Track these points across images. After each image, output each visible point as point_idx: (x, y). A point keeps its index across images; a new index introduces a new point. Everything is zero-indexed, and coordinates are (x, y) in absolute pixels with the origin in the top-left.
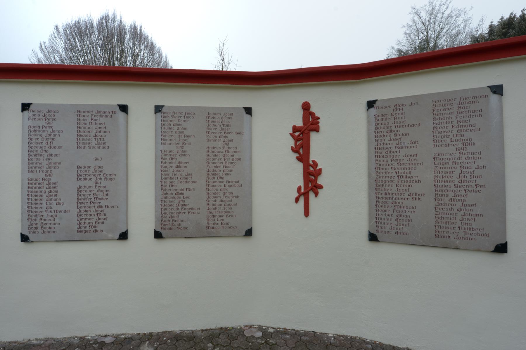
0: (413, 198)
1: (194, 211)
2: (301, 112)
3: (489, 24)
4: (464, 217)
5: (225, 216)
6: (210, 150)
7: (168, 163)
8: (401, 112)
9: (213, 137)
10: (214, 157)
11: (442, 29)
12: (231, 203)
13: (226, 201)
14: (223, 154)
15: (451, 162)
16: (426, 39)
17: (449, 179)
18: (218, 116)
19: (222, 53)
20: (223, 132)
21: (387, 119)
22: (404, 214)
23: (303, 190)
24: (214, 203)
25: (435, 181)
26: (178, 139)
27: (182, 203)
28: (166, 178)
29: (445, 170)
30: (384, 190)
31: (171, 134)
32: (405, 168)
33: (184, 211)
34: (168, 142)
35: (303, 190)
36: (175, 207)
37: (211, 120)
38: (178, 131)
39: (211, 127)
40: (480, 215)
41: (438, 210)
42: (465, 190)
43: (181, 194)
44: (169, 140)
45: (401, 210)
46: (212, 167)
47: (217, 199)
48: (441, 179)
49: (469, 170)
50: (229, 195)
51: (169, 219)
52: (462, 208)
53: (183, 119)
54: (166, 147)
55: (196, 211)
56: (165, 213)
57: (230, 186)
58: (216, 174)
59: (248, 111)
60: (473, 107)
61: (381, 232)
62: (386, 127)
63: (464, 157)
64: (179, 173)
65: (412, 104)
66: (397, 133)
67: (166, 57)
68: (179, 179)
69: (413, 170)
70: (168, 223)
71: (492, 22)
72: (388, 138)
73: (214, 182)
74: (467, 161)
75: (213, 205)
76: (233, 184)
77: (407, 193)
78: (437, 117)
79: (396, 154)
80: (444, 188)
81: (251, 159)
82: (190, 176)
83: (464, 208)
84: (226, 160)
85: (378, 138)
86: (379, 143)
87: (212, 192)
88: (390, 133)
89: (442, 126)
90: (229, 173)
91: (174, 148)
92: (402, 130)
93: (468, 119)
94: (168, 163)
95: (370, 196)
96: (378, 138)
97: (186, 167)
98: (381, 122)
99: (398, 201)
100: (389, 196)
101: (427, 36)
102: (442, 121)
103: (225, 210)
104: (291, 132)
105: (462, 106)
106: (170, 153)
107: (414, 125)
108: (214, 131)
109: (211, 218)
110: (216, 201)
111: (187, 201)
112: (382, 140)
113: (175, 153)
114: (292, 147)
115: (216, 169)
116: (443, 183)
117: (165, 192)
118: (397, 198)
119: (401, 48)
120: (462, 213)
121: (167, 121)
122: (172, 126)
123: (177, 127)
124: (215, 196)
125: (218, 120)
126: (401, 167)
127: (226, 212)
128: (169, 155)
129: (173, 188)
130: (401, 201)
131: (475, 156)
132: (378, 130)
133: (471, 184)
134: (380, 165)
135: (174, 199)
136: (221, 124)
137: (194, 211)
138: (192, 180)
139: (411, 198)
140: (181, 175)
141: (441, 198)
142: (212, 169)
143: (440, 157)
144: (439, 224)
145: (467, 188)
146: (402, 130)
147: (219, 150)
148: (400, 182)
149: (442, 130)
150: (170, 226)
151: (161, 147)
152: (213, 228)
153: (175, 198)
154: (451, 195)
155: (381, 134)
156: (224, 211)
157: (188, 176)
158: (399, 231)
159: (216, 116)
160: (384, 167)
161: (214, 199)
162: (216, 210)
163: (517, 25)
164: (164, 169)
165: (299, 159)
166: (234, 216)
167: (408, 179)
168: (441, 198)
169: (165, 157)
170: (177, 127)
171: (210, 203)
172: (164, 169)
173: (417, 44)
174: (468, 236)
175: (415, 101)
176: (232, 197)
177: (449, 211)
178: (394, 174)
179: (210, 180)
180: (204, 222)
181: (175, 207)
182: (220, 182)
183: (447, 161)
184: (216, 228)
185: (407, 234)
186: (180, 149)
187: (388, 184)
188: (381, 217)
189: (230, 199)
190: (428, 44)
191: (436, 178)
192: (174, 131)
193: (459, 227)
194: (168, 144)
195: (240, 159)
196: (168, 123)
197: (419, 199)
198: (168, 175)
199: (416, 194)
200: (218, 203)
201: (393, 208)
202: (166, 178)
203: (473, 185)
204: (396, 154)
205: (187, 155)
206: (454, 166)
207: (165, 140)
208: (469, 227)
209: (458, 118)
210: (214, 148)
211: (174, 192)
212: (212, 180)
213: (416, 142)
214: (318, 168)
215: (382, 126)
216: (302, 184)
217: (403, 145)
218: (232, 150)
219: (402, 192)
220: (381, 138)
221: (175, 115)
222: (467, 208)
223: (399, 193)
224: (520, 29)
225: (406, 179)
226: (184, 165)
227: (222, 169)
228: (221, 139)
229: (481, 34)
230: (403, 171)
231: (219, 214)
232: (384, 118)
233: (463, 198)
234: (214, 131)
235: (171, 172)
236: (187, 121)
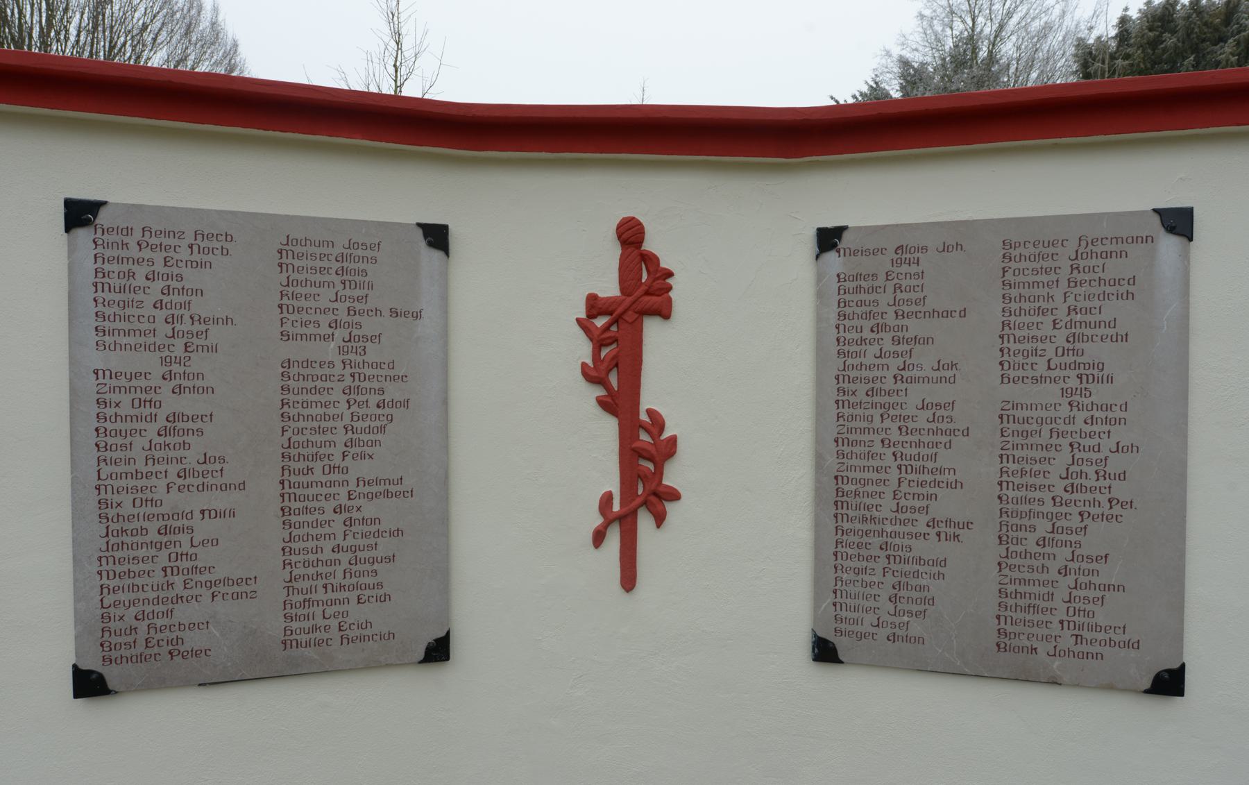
0: (939, 535)
1: (236, 589)
2: (613, 252)
3: (1119, 14)
4: (1075, 593)
5: (354, 600)
6: (294, 371)
7: (125, 419)
8: (914, 269)
9: (305, 324)
10: (310, 398)
11: (1009, 15)
12: (373, 553)
13: (355, 549)
14: (342, 385)
15: (1046, 430)
16: (971, 37)
17: (1039, 481)
18: (325, 250)
19: (393, 17)
20: (342, 307)
21: (874, 289)
22: (913, 582)
23: (616, 507)
24: (312, 557)
25: (1000, 484)
26: (168, 329)
27: (185, 564)
28: (119, 476)
29: (1031, 454)
30: (858, 507)
31: (138, 312)
32: (919, 444)
33: (195, 592)
34: (124, 340)
35: (616, 507)
36: (158, 577)
37: (297, 263)
38: (166, 299)
39: (299, 290)
40: (1118, 588)
41: (1006, 571)
42: (1081, 514)
43: (181, 530)
44: (127, 333)
45: (907, 568)
46: (300, 431)
47: (321, 543)
48: (1017, 481)
49: (1094, 456)
50: (366, 528)
51: (135, 623)
52: (1070, 565)
53: (184, 254)
54: (115, 361)
55: (242, 588)
56: (115, 604)
57: (371, 497)
58: (316, 457)
59: (437, 236)
60: (1115, 268)
61: (849, 634)
62: (869, 315)
63: (1081, 416)
64: (172, 454)
65: (945, 248)
66: (900, 334)
67: (216, 10)
68: (172, 477)
69: (941, 451)
70: (130, 639)
71: (1126, 9)
72: (873, 350)
73: (309, 485)
74: (1087, 428)
75: (307, 564)
76: (381, 488)
77: (923, 519)
78: (1014, 293)
79: (894, 399)
80: (1026, 508)
81: (445, 402)
82: (218, 466)
83: (1075, 565)
84: (354, 408)
85: (846, 348)
86: (850, 361)
87: (302, 518)
88: (882, 335)
89: (1027, 319)
90: (368, 450)
91: (150, 362)
92: (915, 327)
93: (1097, 303)
94: (125, 419)
95: (818, 526)
96: (846, 348)
97: (200, 432)
98: (856, 297)
99: (897, 541)
100: (872, 527)
101: (973, 29)
102: (1026, 306)
103: (354, 580)
104: (583, 315)
105: (1082, 263)
106: (134, 383)
107: (949, 314)
108: (311, 303)
109: (300, 612)
110: (317, 550)
111: (205, 556)
112: (858, 354)
113: (155, 381)
114: (584, 365)
115: (318, 438)
116: (1023, 493)
117: (113, 526)
118: (897, 534)
119: (908, 55)
120: (1070, 580)
121: (119, 260)
122: (140, 281)
123: (159, 284)
124: (314, 532)
125: (325, 264)
126: (909, 438)
127: (357, 586)
128: (128, 390)
129: (150, 510)
130: (906, 542)
131: (1110, 415)
132: (846, 322)
133: (1098, 496)
134: (850, 431)
135: (153, 552)
136: (337, 279)
137: (236, 589)
138: (226, 479)
139: (933, 532)
140: (180, 460)
141: (1015, 534)
142: (301, 438)
143: (1019, 414)
144: (1008, 613)
145: (1087, 508)
146: (915, 327)
147: (327, 371)
148: (905, 484)
149: (1024, 332)
150: (140, 648)
151: (98, 360)
152: (308, 644)
153: (158, 546)
154: (1043, 527)
155: (855, 336)
156: (347, 582)
157: (210, 467)
158: (898, 632)
159: (318, 251)
160: (862, 437)
161: (311, 544)
162: (320, 582)
163: (1181, 23)
164: (110, 441)
165: (608, 405)
166: (386, 598)
167: (929, 478)
168: (1015, 534)
169: (115, 397)
170: (159, 284)
171: (294, 558)
172: (110, 441)
173: (947, 48)
174: (1084, 648)
175: (955, 238)
176: (380, 534)
177: (1036, 576)
178: (889, 460)
179: (293, 479)
180: (275, 625)
181: (158, 577)
182: (332, 484)
183: (1035, 427)
184: (319, 643)
185: (919, 640)
186: (176, 368)
187: (870, 488)
188: (850, 588)
189: (372, 541)
190: (975, 50)
191: (1005, 477)
192: (149, 301)
193: (1061, 622)
194: (123, 347)
195: (405, 404)
196: (125, 268)
197: (956, 537)
198: (128, 462)
199: (948, 522)
200: (327, 555)
201: (883, 562)
202: (119, 476)
203: (1103, 499)
204: (894, 399)
205: (205, 390)
206: (1054, 441)
207: (111, 332)
208: (1086, 620)
209: (1071, 300)
210: (309, 363)
211: (153, 526)
212: (302, 478)
213: (953, 365)
214: (666, 435)
215: (859, 310)
216: (615, 489)
217: (915, 373)
218: (379, 372)
219: (908, 515)
220: (854, 348)
221: (154, 241)
222: (1084, 565)
223: (902, 516)
224: (1188, 35)
225: (922, 477)
226: (190, 425)
227: (340, 437)
228: (337, 333)
229: (1099, 38)
230: (914, 451)
231: (331, 595)
232: (864, 284)
233: (1073, 538)
234: (311, 303)
235: (138, 453)
236: (203, 265)
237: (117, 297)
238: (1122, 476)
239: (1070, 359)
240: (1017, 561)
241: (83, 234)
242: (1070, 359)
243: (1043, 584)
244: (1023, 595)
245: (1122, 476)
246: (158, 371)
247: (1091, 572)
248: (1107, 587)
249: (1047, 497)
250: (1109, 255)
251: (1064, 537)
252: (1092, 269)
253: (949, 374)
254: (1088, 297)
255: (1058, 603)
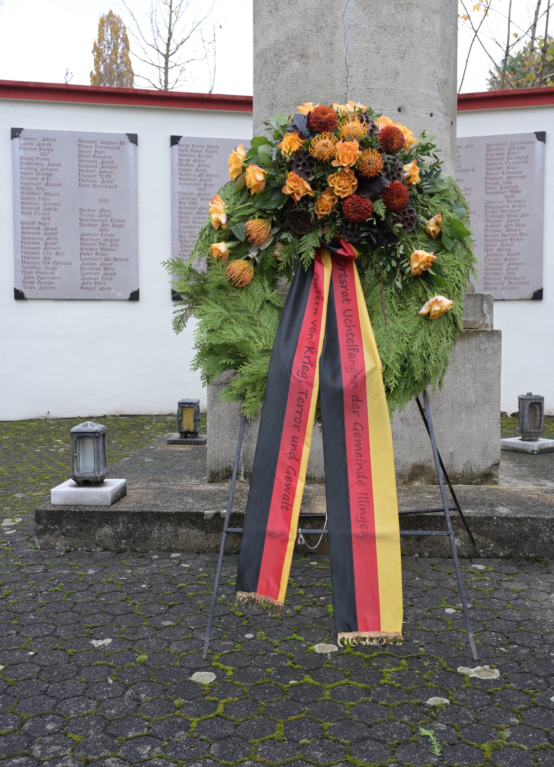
7: (187, 208)
15: (500, 211)
28: (185, 227)
34: (187, 182)
40: (523, 264)
44: (188, 180)
49: (515, 218)
53: (204, 153)
54: (185, 189)
60: (522, 153)
63: (511, 205)
74: (513, 209)
78: (490, 162)
93: (516, 165)
94: (187, 208)
102: (494, 167)
105: (512, 151)
107: (468, 170)
117: (184, 244)
120: (507, 263)
121: (186, 155)
122: (191, 162)
123: (197, 164)
128: (188, 199)
133: (516, 233)
143: (492, 205)
149: (493, 176)
151: (179, 189)
154: (499, 244)
169: (184, 201)
170: (197, 164)
177: (496, 262)
183: (496, 209)
186: (202, 192)
192: (194, 169)
194: (187, 184)
202: (185, 227)
203: (518, 233)
207: (183, 180)
209: (508, 165)
221: (196, 149)
233: (509, 247)
235: (190, 220)
237: (185, 168)
238: (524, 225)
239: (507, 185)
240: (491, 257)
241: (175, 147)
242: (507, 185)
243: (498, 264)
244: (492, 269)
245: (524, 225)
246: (197, 192)
247: (514, 259)
248: (519, 264)
249: (500, 234)
250: (520, 148)
251: (506, 248)
252: (515, 153)
253: (468, 192)
254: (514, 163)
255: (504, 271)
